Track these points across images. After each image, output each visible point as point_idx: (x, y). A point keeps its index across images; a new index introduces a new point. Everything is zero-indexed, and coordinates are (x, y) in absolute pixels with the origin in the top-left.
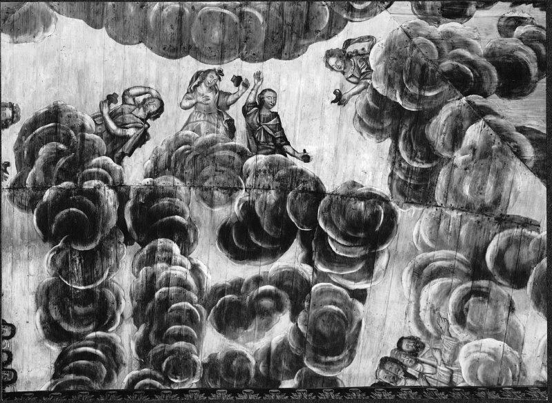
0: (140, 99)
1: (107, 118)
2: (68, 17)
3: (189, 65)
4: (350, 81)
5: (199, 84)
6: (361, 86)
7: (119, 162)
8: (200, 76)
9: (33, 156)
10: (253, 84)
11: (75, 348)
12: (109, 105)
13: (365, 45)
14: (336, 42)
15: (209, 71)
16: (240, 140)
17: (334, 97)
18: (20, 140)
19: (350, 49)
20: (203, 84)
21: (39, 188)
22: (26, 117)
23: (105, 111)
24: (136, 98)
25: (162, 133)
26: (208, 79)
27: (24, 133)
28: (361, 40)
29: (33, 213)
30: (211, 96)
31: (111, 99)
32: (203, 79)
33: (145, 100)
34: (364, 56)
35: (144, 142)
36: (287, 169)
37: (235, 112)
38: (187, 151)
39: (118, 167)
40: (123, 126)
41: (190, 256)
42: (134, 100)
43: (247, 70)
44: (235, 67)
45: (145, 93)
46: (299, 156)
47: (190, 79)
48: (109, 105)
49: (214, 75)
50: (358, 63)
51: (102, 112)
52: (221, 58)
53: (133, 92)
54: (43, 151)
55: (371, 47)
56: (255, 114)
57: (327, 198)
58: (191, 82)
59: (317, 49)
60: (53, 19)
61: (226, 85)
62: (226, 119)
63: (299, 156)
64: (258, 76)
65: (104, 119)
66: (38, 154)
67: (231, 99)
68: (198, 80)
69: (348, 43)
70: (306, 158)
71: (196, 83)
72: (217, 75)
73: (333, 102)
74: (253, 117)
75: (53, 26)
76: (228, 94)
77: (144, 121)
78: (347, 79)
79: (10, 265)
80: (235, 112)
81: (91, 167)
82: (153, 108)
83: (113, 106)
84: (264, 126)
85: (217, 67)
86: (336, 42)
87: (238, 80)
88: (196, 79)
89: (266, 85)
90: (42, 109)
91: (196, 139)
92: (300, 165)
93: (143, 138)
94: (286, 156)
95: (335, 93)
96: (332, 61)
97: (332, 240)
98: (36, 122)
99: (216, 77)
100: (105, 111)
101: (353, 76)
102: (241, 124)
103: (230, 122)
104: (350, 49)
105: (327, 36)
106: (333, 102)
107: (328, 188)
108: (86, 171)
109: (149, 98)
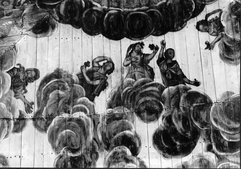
0: (101, 64)
1: (85, 75)
2: (63, 24)
3: (126, 42)
4: (212, 35)
5: (132, 51)
6: (220, 36)
7: (92, 100)
8: (132, 47)
9: (46, 98)
10: (161, 47)
11: (142, 89)
12: (86, 67)
13: (217, 14)
14: (201, 17)
15: (136, 44)
16: (158, 79)
17: (206, 46)
18: (40, 89)
19: (209, 18)
20: (134, 51)
21: (50, 118)
22: (42, 76)
23: (84, 71)
24: (100, 63)
25: (114, 80)
26: (137, 48)
27: (42, 84)
28: (214, 12)
29: (46, 133)
30: (139, 57)
31: (87, 64)
32: (134, 49)
33: (104, 64)
34: (217, 21)
35: (105, 88)
36: (187, 93)
37: (153, 63)
38: (129, 91)
39: (92, 103)
40: (92, 79)
41: (138, 156)
42: (98, 64)
43: (156, 40)
44: (148, 41)
45: (104, 60)
46: (192, 83)
47: (127, 50)
48: (86, 67)
49: (139, 45)
50: (215, 24)
51: (82, 72)
52: (142, 37)
53: (97, 60)
54: (51, 96)
55: (220, 15)
56: (164, 63)
57: (214, 106)
58: (128, 51)
59: (192, 24)
60: (56, 25)
61: (146, 50)
62: (148, 69)
63: (192, 83)
64: (163, 44)
65: (83, 76)
66: (49, 97)
67: (149, 57)
68: (131, 49)
69: (208, 16)
70: (197, 84)
71: (130, 51)
72: (140, 45)
73: (206, 49)
74: (163, 66)
75: (56, 29)
76: (148, 55)
77: (105, 75)
78: (211, 35)
79: (77, 79)
80: (153, 63)
81: (77, 104)
82: (108, 68)
83: (88, 68)
84: (170, 69)
85: (140, 41)
86: (201, 17)
87: (152, 47)
88: (130, 49)
89: (167, 47)
90: (51, 71)
91: (133, 83)
92: (194, 88)
93: (104, 86)
94: (185, 85)
95: (206, 43)
96: (201, 27)
97: (223, 132)
98: (47, 79)
99: (140, 47)
100: (84, 71)
101: (214, 32)
102: (157, 71)
103: (151, 70)
104: (209, 18)
105: (195, 15)
106: (206, 49)
107: (214, 100)
108: (75, 106)
109: (106, 63)
